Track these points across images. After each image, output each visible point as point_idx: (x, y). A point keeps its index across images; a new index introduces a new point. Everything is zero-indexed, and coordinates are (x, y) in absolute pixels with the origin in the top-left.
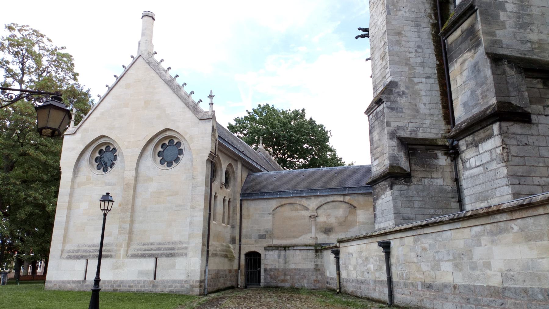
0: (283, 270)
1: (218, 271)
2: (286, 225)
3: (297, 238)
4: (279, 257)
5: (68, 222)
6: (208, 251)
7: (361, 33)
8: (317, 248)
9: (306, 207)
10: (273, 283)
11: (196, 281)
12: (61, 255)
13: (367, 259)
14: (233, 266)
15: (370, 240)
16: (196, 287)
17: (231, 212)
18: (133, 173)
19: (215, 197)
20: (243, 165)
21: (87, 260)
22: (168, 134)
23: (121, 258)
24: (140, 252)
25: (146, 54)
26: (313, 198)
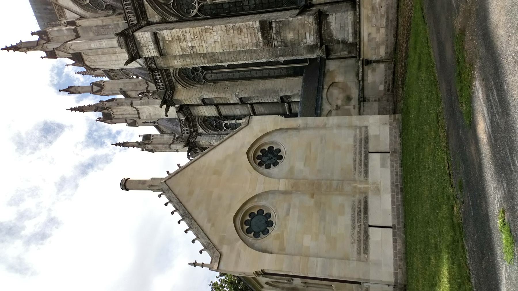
16: (395, 116)
26: (323, 107)
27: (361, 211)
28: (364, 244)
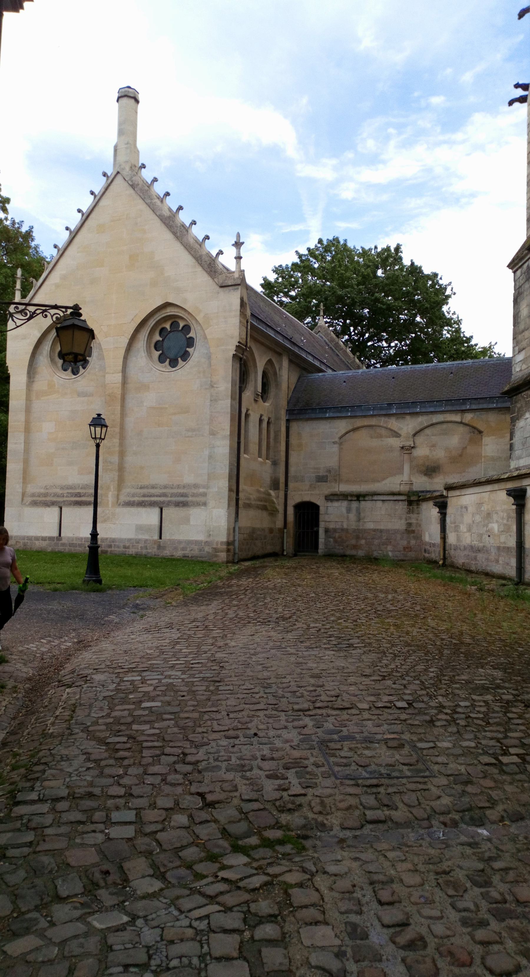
0: (354, 531)
1: (254, 530)
2: (361, 459)
3: (379, 481)
4: (349, 510)
5: (27, 450)
6: (237, 500)
7: (520, 92)
8: (412, 498)
9: (395, 432)
10: (339, 550)
11: (222, 543)
12: (23, 500)
13: (489, 515)
14: (275, 523)
15: (496, 486)
16: (222, 551)
17: (272, 440)
18: (118, 377)
19: (247, 415)
20: (291, 361)
21: (61, 508)
22: (170, 311)
23: (110, 506)
24: (136, 499)
25: (128, 168)
26: (408, 417)
27: (80, 496)
28: (40, 502)
